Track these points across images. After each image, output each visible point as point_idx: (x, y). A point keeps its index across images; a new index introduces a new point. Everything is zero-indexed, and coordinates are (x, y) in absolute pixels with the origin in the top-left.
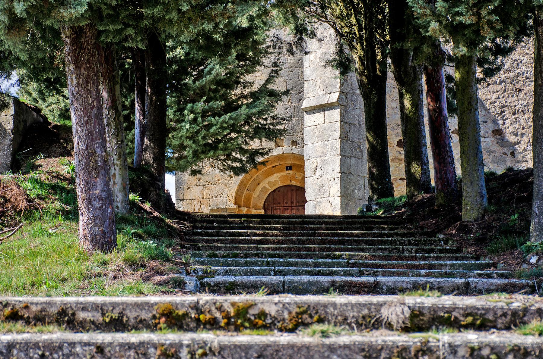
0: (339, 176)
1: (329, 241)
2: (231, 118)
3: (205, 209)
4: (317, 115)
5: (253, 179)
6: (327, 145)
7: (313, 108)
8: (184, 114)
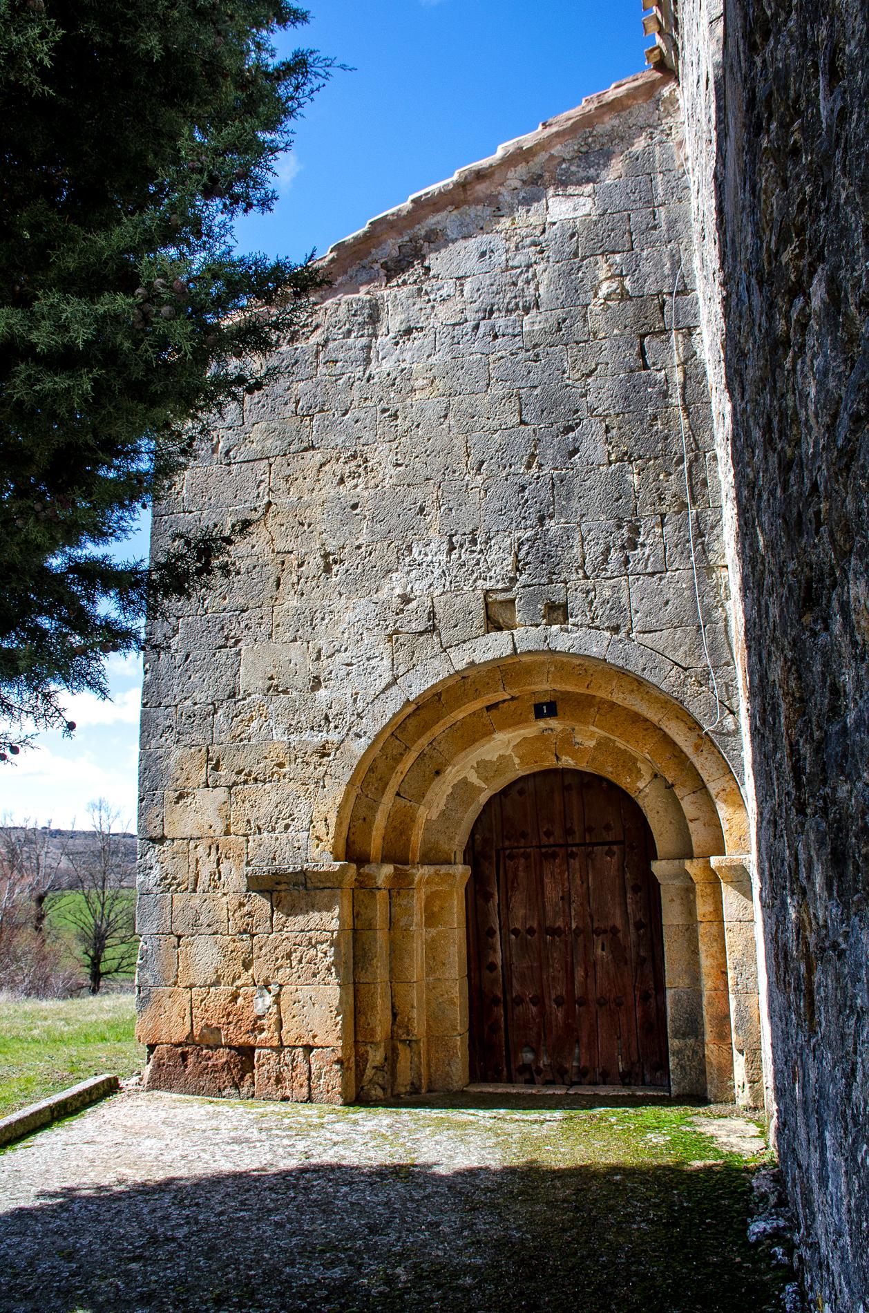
3: (234, 875)
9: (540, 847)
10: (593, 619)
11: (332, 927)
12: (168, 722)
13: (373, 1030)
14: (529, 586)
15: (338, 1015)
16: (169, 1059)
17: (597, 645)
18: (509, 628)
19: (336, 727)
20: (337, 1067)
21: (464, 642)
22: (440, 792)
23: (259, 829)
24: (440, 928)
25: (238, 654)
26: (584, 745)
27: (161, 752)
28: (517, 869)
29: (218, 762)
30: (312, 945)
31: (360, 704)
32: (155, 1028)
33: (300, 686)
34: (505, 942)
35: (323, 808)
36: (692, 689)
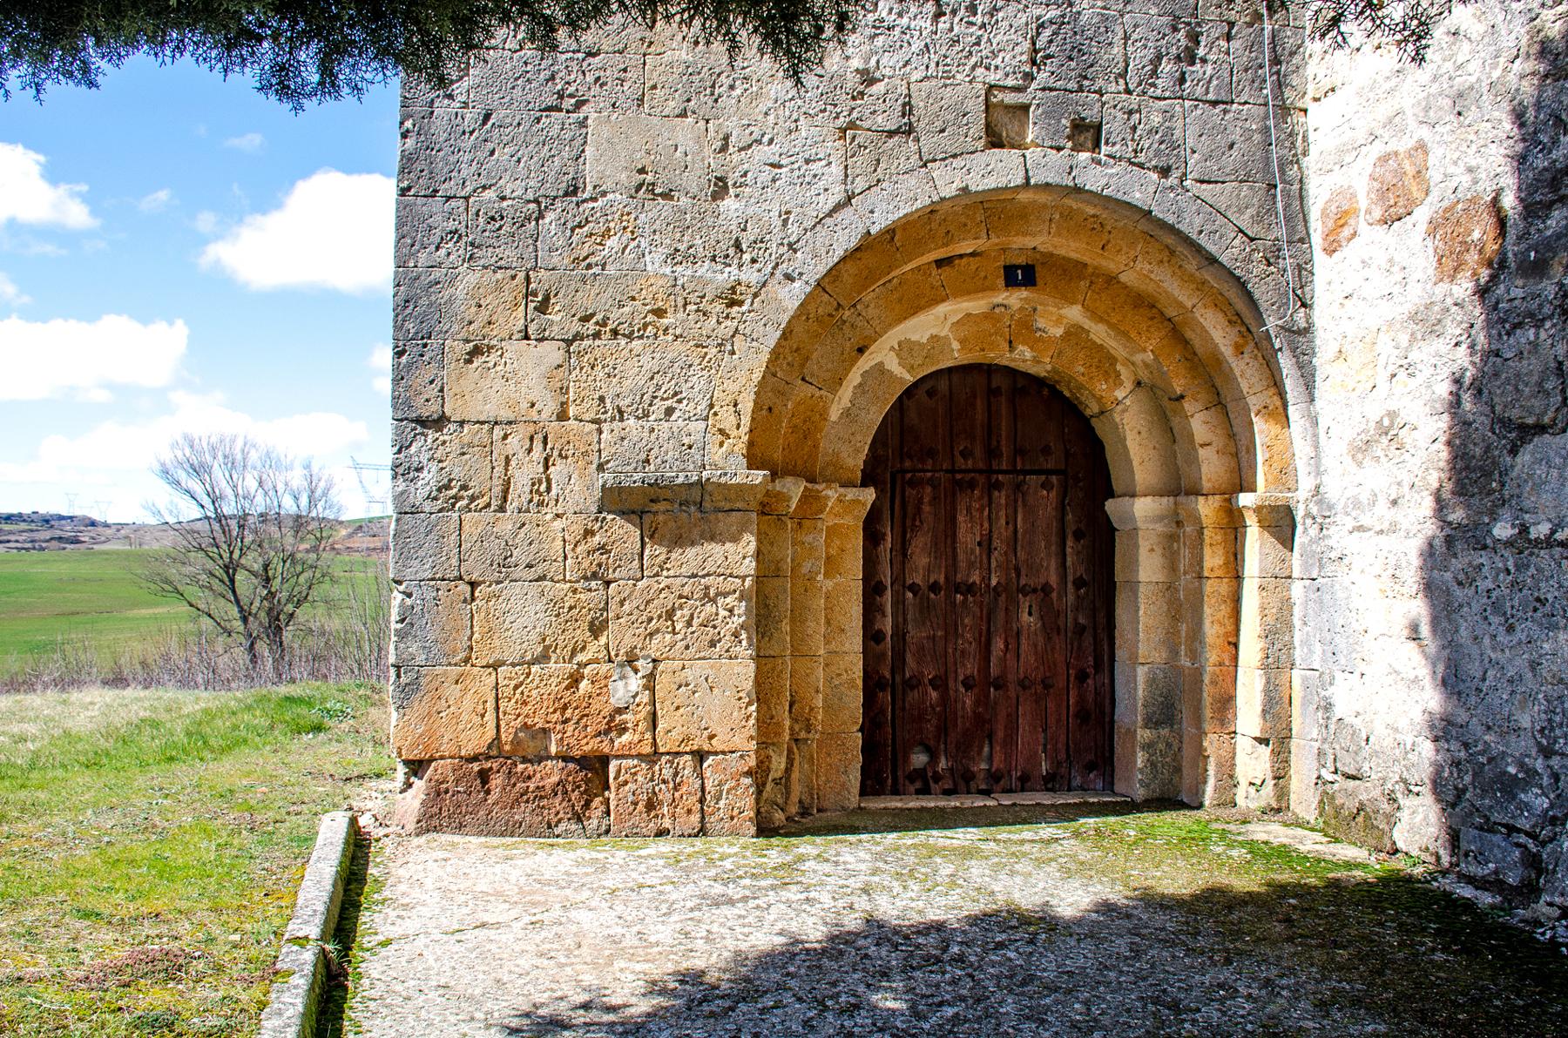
10: (1135, 151)
11: (743, 571)
12: (452, 225)
14: (1051, 89)
15: (749, 704)
16: (457, 782)
17: (1141, 190)
18: (1019, 147)
19: (754, 261)
20: (748, 781)
21: (954, 156)
23: (621, 412)
25: (583, 124)
26: (1048, 333)
27: (437, 274)
28: (920, 501)
29: (547, 299)
30: (708, 598)
31: (794, 230)
32: (430, 733)
33: (694, 190)
34: (899, 602)
35: (731, 387)
36: (1259, 268)
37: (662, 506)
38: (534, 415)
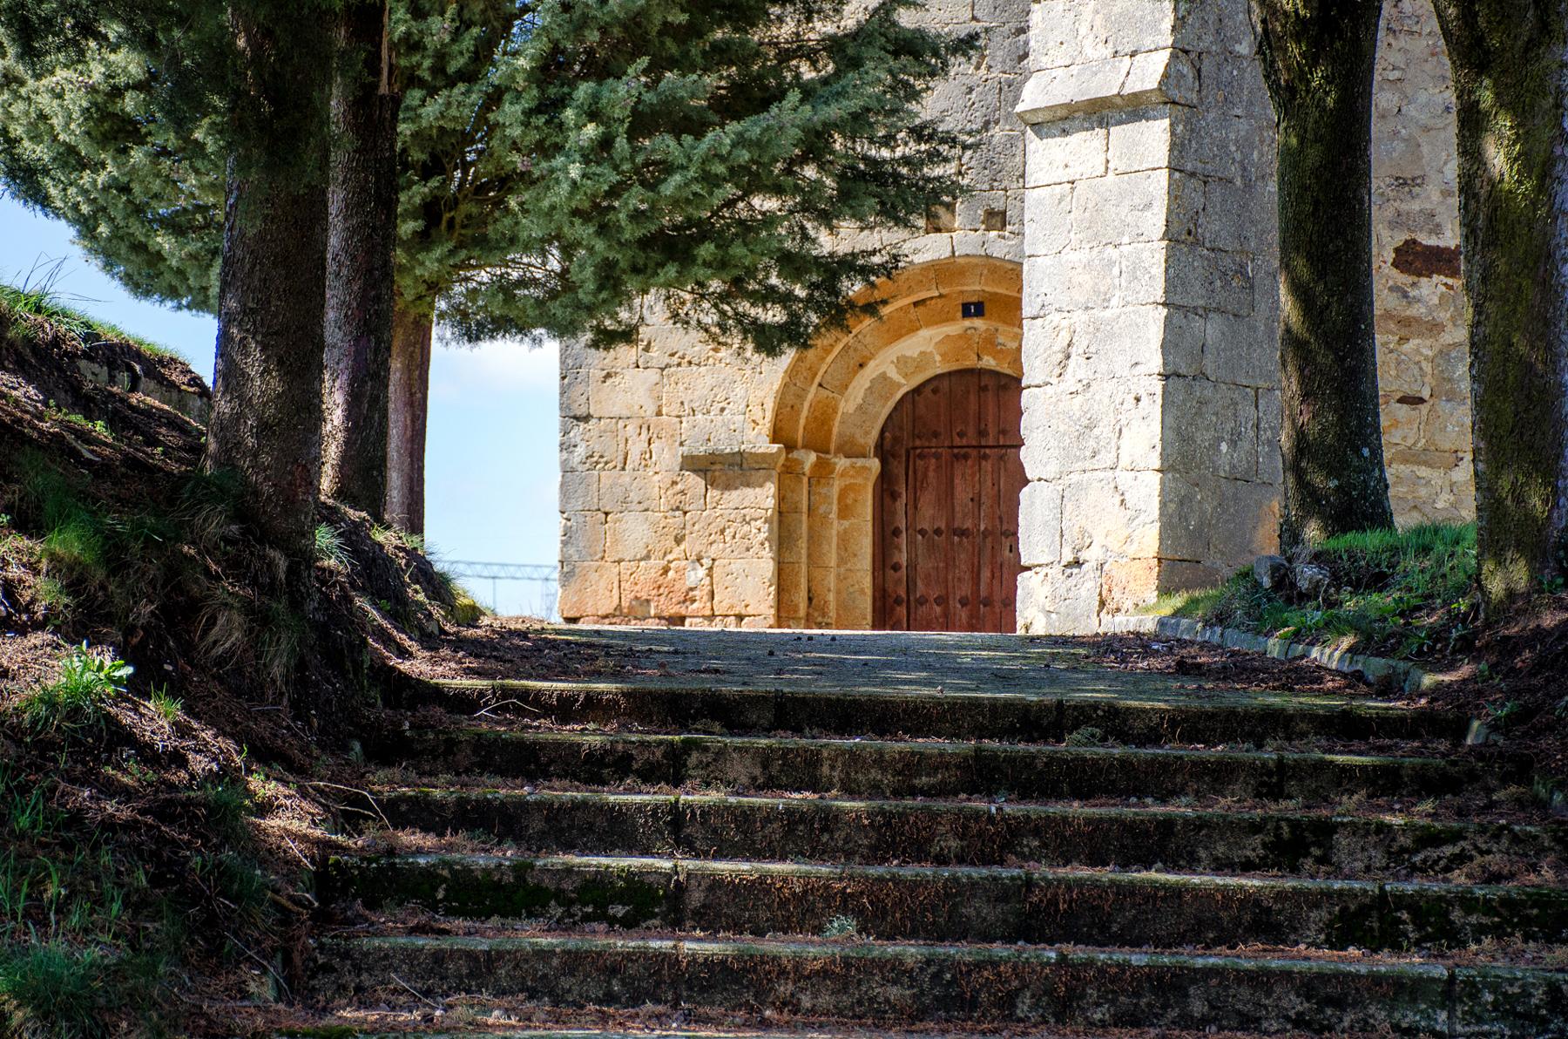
0: (1157, 386)
1: (1102, 971)
2: (740, 141)
3: (666, 455)
4: (1077, 138)
5: (841, 346)
6: (1111, 263)
7: (1064, 113)
8: (561, 124)
9: (952, 447)
13: (797, 606)
22: (861, 383)
24: (853, 520)
28: (927, 469)
34: (911, 543)
35: (760, 394)
37: (718, 467)
38: (642, 412)
